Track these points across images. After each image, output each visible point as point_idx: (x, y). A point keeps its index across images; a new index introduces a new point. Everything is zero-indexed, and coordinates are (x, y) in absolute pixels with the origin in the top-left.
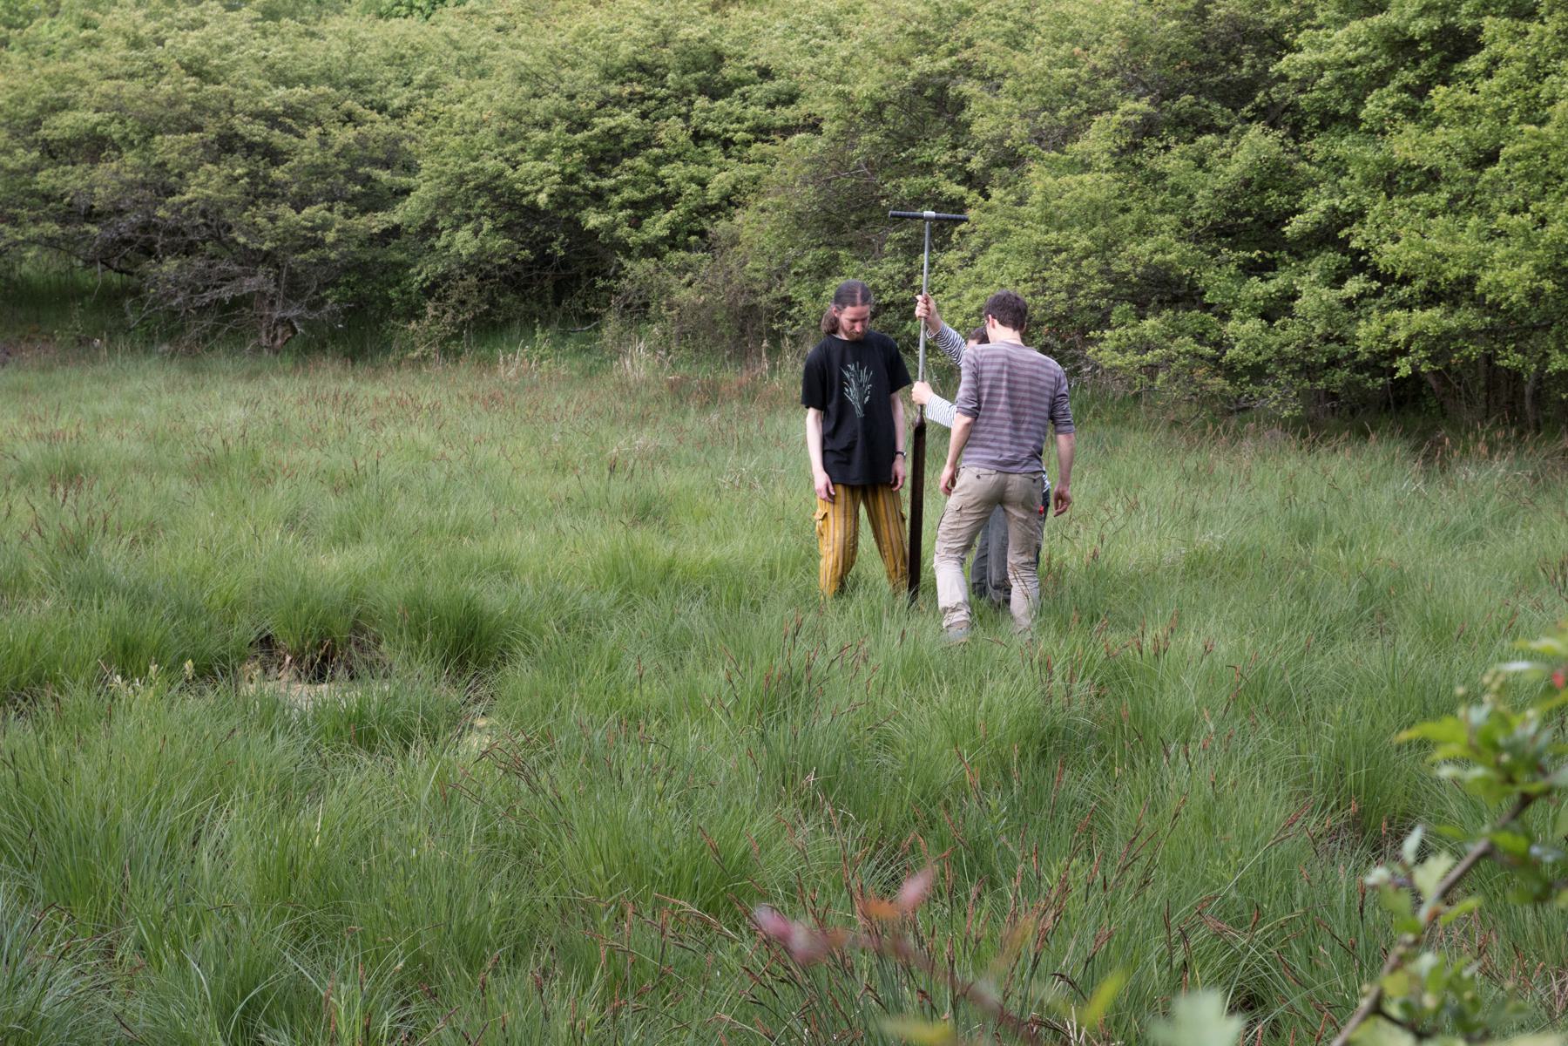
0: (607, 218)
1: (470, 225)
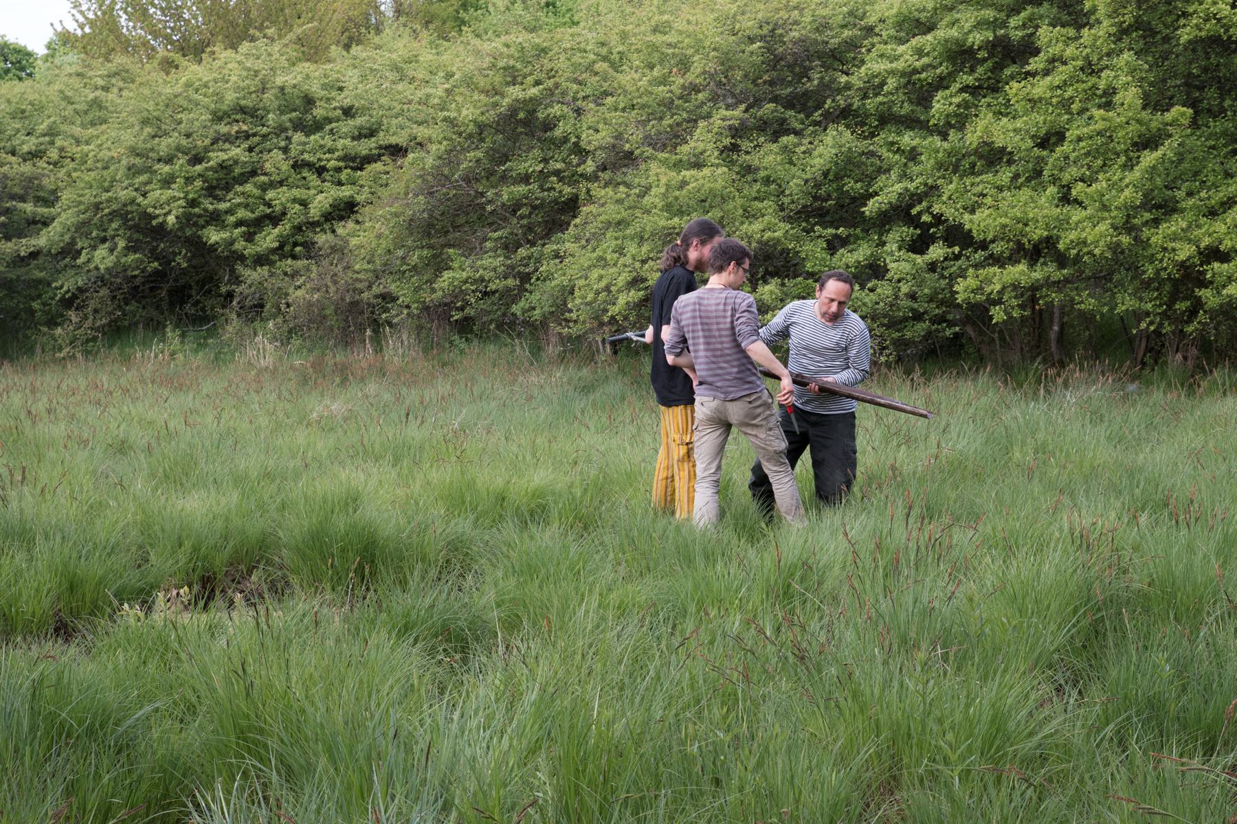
0: (225, 235)
1: (107, 245)
